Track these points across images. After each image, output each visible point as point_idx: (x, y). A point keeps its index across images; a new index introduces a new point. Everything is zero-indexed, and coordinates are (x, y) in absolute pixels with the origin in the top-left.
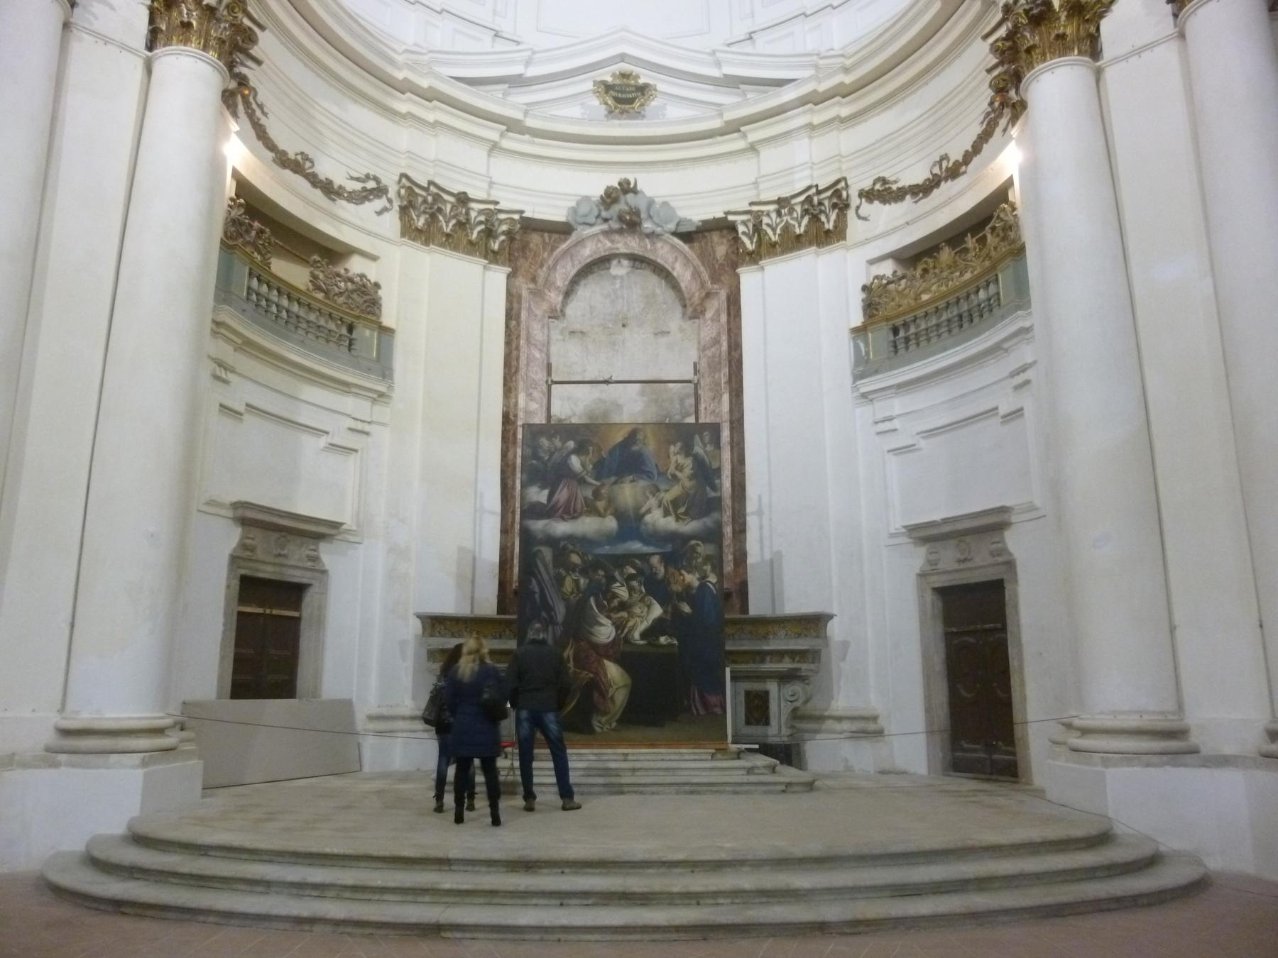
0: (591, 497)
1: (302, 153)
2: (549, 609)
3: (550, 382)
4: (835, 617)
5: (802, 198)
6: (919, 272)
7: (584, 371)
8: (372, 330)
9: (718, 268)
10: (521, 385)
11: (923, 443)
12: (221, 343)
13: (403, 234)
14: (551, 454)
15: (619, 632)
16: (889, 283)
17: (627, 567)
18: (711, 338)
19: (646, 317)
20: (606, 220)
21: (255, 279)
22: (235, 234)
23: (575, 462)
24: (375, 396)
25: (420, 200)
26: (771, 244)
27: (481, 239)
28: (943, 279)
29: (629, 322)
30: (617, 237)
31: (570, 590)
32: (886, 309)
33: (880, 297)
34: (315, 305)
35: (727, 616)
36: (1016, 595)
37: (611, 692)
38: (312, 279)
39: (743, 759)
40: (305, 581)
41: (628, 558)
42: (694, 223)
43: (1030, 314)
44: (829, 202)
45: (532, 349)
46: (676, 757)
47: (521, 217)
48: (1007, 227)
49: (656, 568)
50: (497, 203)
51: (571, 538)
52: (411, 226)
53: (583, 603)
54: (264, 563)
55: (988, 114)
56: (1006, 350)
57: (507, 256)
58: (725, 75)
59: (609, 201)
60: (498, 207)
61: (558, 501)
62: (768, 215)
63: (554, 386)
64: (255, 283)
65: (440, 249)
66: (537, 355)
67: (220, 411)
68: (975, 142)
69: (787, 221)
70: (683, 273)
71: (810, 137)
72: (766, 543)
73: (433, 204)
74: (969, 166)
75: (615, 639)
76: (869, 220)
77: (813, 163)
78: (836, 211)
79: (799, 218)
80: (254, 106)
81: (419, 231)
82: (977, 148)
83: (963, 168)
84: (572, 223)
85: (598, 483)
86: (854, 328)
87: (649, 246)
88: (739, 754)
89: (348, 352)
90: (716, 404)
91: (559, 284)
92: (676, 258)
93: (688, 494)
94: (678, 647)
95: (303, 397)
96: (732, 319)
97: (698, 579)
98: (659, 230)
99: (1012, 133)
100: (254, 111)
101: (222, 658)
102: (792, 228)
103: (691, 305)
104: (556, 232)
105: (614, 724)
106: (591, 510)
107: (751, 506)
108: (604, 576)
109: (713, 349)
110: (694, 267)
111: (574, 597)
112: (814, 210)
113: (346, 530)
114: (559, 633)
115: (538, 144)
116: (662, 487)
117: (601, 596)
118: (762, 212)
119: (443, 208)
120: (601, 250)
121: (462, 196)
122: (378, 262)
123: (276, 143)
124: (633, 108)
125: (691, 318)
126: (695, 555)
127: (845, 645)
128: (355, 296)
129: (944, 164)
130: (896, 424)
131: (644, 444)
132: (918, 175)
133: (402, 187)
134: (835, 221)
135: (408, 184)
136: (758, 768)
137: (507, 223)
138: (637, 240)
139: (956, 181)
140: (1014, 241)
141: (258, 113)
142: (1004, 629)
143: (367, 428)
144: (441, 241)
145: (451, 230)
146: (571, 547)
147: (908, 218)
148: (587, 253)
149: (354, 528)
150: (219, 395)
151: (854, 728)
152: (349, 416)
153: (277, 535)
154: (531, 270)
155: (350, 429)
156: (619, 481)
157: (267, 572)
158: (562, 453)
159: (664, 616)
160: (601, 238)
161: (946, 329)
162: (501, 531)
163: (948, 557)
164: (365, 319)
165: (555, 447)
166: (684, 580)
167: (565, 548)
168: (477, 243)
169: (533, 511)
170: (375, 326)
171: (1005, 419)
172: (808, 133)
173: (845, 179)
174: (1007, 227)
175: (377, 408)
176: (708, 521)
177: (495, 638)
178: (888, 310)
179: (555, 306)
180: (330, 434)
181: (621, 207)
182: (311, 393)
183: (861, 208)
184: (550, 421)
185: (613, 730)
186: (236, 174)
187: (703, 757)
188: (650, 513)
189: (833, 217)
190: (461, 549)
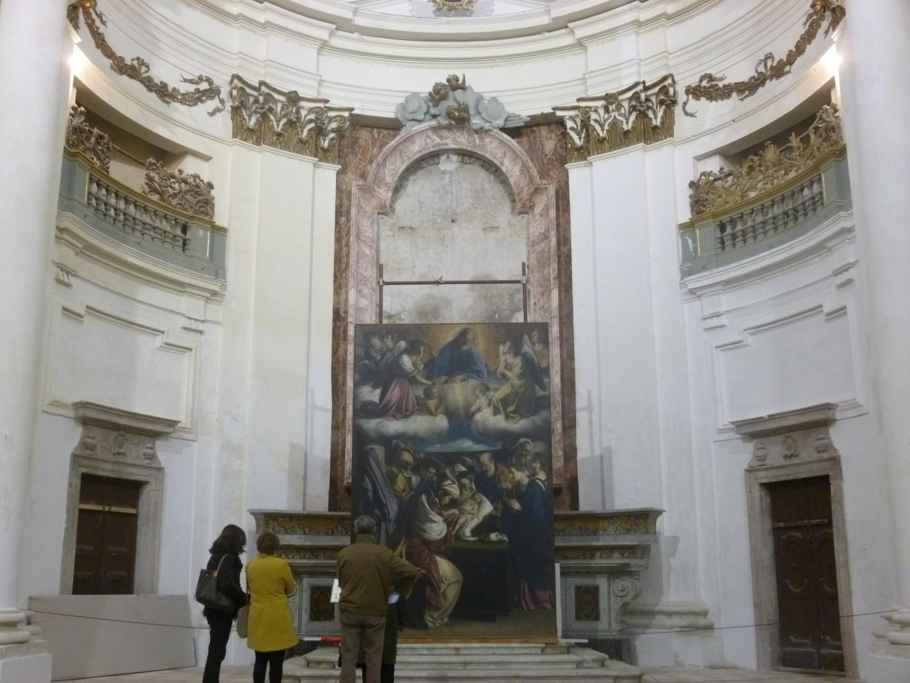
0: (423, 396)
1: (138, 59)
2: (382, 506)
3: (381, 283)
4: (664, 513)
5: (629, 94)
6: (745, 170)
7: (414, 267)
8: (206, 229)
9: (547, 163)
10: (351, 282)
11: (750, 340)
12: (65, 250)
13: (235, 135)
14: (383, 355)
15: (451, 528)
16: (715, 180)
17: (458, 465)
18: (540, 233)
19: (475, 212)
20: (435, 117)
21: (95, 184)
22: (76, 142)
23: (407, 362)
24: (209, 295)
25: (252, 99)
26: (599, 140)
27: (311, 137)
28: (769, 176)
29: (458, 217)
30: (446, 133)
31: (402, 487)
32: (713, 205)
33: (707, 194)
34: (151, 207)
35: (556, 512)
36: (841, 491)
37: (443, 587)
38: (148, 181)
39: (572, 654)
40: (142, 478)
41: (459, 456)
42: (522, 119)
43: (851, 215)
44: (656, 98)
45: (362, 244)
46: (507, 652)
47: (351, 115)
48: (829, 128)
49: (486, 465)
50: (327, 101)
51: (402, 436)
52: (242, 125)
53: (416, 498)
54: (104, 461)
55: (811, 16)
56: (830, 250)
57: (337, 153)
58: (553, 19)
59: (437, 97)
60: (327, 105)
61: (389, 401)
62: (596, 111)
63: (385, 288)
64: (94, 187)
65: (272, 148)
66: (367, 252)
67: (63, 313)
68: (798, 42)
69: (615, 116)
70: (512, 170)
71: (637, 33)
72: (596, 438)
73: (263, 104)
74: (794, 65)
75: (446, 535)
76: (696, 117)
77: (640, 59)
78: (664, 107)
79: (627, 114)
80: (94, 16)
81: (251, 131)
82: (800, 49)
83: (787, 68)
84: (402, 119)
85: (429, 383)
86: (682, 224)
87: (478, 142)
88: (568, 649)
89: (182, 252)
90: (546, 299)
91: (388, 181)
92: (505, 153)
93: (516, 392)
94: (508, 543)
95: (139, 298)
96: (561, 214)
97: (528, 477)
98: (487, 126)
99: (832, 37)
100: (93, 21)
101: (65, 554)
102: (620, 124)
103: (520, 200)
104: (386, 128)
105: (446, 620)
106: (423, 409)
107: (581, 402)
108: (435, 474)
109: (542, 245)
110: (523, 162)
111: (406, 495)
112: (642, 106)
113: (182, 428)
114: (391, 530)
115: (367, 42)
116: (492, 386)
117: (432, 492)
118: (591, 108)
119: (274, 107)
120: (430, 145)
121: (293, 95)
122: (211, 162)
123: (113, 50)
124: (461, 5)
125: (520, 213)
126: (524, 453)
127: (675, 540)
128: (188, 197)
129: (769, 63)
130: (723, 320)
131: (474, 344)
132: (743, 73)
133: (234, 88)
134: (662, 118)
135: (240, 85)
136: (586, 661)
137: (336, 121)
138: (466, 136)
139: (781, 79)
140: (836, 143)
141: (98, 22)
142: (830, 524)
143: (201, 327)
144: (272, 140)
145: (282, 129)
146: (403, 445)
147: (735, 115)
148: (416, 149)
149: (189, 426)
150: (61, 298)
151: (684, 624)
152: (183, 315)
153: (115, 433)
154: (360, 166)
155: (185, 328)
156: (450, 381)
157: (106, 470)
158: (394, 353)
159: (494, 513)
160: (430, 133)
161: (772, 226)
162: (332, 428)
163: (776, 452)
164: (200, 220)
165: (387, 347)
166: (513, 478)
167: (397, 446)
168: (307, 141)
169: (364, 410)
170: (209, 226)
171: (829, 317)
172: (635, 29)
173: (672, 76)
174: (829, 128)
175: (211, 307)
176: (537, 419)
177: (327, 534)
178: (715, 207)
179: (384, 203)
180: (166, 333)
181: (450, 103)
182: (148, 293)
183: (688, 104)
184: (382, 322)
185: (446, 625)
186: (77, 83)
187: (534, 651)
188: (480, 411)
189: (660, 113)
190: (293, 446)
